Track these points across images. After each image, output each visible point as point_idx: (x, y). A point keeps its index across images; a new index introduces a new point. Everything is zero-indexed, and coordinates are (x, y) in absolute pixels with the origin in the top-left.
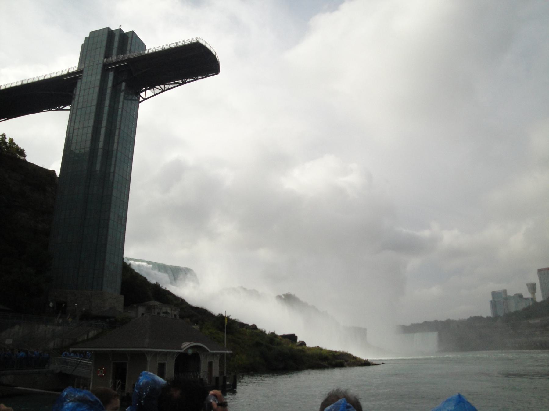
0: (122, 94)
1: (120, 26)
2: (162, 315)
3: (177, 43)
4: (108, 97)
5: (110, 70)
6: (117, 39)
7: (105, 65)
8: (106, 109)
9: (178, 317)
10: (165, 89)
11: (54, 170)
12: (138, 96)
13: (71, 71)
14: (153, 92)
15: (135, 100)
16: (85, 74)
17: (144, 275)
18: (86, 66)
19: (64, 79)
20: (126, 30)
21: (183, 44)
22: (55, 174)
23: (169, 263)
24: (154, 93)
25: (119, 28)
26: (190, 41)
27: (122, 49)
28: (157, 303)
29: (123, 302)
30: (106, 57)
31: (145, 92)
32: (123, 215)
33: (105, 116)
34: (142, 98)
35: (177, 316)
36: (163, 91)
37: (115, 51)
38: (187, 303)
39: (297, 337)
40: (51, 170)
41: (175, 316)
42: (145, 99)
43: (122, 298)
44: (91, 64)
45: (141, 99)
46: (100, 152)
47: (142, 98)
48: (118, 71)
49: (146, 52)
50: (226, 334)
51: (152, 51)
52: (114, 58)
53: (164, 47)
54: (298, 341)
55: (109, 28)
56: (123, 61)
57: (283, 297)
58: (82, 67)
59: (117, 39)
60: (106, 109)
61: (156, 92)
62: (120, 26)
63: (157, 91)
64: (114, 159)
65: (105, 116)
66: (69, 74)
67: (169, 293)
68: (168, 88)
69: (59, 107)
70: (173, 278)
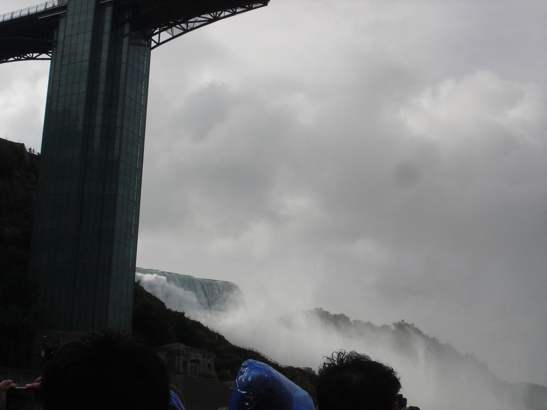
0: (126, 40)
2: (189, 364)
4: (105, 47)
5: (107, 4)
9: (214, 367)
10: (189, 28)
11: (22, 143)
12: (149, 41)
15: (144, 45)
16: (70, 11)
17: (160, 296)
22: (25, 148)
23: (199, 274)
28: (182, 347)
31: (158, 34)
32: (132, 222)
35: (212, 365)
36: (186, 31)
38: (227, 342)
39: (405, 400)
40: (19, 144)
41: (209, 365)
42: (158, 44)
45: (153, 44)
46: (98, 131)
54: (408, 405)
60: (104, 66)
61: (175, 34)
63: (176, 31)
64: (117, 141)
66: (46, 11)
67: (198, 325)
68: (192, 27)
69: (31, 54)
70: (204, 300)
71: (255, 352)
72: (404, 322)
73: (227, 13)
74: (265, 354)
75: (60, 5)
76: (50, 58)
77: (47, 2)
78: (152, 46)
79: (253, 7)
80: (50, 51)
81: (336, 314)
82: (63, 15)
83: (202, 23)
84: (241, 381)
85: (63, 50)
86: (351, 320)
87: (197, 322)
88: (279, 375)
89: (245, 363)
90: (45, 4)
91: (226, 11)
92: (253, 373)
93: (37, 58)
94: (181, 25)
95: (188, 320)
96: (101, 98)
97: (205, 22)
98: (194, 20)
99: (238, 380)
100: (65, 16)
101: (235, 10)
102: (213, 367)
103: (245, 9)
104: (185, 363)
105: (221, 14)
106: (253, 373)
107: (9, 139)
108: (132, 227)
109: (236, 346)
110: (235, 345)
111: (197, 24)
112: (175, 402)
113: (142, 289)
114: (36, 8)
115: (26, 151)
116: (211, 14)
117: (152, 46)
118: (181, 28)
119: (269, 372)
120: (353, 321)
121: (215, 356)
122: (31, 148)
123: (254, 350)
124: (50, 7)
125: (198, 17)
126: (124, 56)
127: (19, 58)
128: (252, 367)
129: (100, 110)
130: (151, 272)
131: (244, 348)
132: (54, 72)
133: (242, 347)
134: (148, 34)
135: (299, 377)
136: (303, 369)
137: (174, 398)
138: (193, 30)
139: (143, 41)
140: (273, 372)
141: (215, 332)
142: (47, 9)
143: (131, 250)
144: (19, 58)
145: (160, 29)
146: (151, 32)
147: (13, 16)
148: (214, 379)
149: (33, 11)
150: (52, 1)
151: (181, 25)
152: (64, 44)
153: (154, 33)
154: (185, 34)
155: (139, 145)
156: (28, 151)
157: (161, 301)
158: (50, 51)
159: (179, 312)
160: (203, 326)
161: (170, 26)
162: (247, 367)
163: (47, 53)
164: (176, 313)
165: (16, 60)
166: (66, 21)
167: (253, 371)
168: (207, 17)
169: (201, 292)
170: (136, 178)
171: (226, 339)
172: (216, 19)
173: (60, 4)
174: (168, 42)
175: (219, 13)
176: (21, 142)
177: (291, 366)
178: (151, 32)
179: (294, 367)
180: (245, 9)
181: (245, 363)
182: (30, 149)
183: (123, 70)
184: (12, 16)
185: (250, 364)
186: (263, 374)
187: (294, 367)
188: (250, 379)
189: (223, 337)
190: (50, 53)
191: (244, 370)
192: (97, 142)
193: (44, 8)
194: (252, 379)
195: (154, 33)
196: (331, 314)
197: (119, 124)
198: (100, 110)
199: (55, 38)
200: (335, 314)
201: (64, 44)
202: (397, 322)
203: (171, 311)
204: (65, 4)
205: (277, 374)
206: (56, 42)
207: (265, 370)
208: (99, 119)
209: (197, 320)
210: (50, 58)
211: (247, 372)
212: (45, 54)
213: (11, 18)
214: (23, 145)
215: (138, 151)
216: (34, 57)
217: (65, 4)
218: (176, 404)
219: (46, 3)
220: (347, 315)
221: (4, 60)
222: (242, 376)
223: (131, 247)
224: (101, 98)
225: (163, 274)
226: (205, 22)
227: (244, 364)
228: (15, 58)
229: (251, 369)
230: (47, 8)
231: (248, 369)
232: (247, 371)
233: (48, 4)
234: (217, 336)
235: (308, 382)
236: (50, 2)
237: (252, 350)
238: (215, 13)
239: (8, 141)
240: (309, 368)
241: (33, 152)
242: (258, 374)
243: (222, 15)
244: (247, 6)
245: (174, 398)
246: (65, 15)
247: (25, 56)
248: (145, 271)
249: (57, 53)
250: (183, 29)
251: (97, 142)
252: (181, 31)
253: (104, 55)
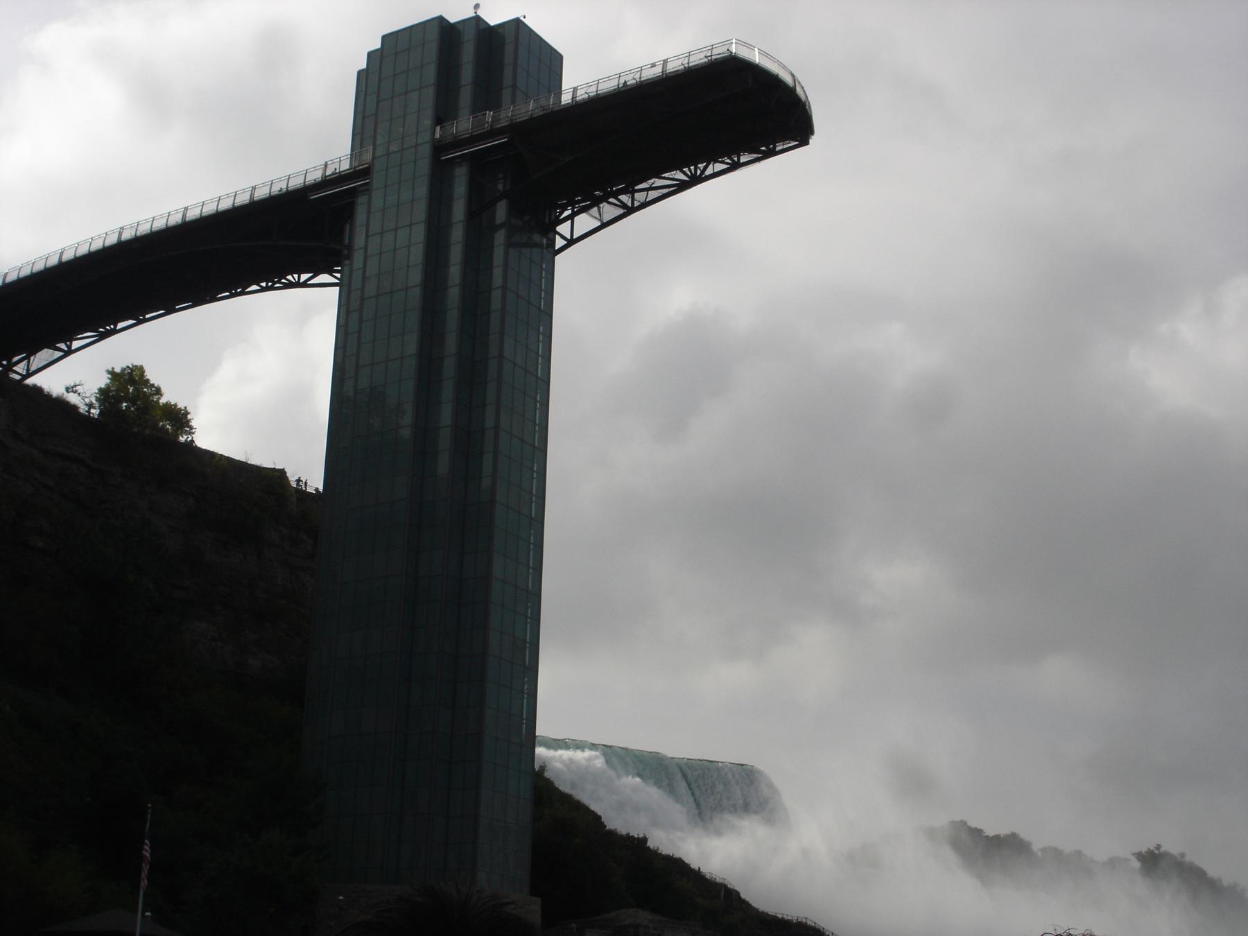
0: (500, 237)
1: (477, 6)
3: (665, 62)
6: (468, 54)
7: (439, 148)
8: (454, 293)
10: (636, 204)
11: (281, 468)
12: (551, 235)
15: (540, 246)
16: (377, 180)
18: (378, 153)
20: (494, 17)
21: (686, 66)
22: (287, 478)
25: (472, 14)
26: (706, 57)
27: (488, 94)
30: (439, 121)
34: (563, 237)
36: (629, 210)
37: (465, 96)
42: (571, 242)
44: (394, 147)
45: (560, 243)
46: (445, 438)
47: (563, 237)
48: (481, 165)
49: (566, 98)
51: (586, 96)
52: (464, 125)
53: (622, 81)
55: (441, 20)
56: (493, 133)
58: (367, 157)
59: (468, 54)
60: (454, 293)
61: (606, 218)
62: (477, 6)
66: (326, 183)
68: (642, 200)
69: (296, 276)
216: (301, 281)
246: (366, 189)
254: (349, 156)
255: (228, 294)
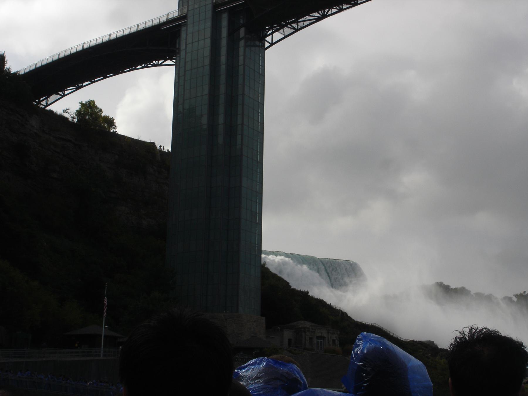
0: (242, 43)
2: (315, 341)
4: (224, 51)
5: (224, 11)
9: (338, 342)
10: (299, 27)
11: (153, 142)
12: (263, 42)
13: (171, 16)
14: (283, 33)
15: (259, 46)
16: (190, 20)
19: (163, 29)
24: (284, 35)
28: (308, 324)
29: (264, 325)
31: (271, 35)
33: (223, 78)
34: (268, 42)
35: (336, 341)
36: (296, 30)
40: (150, 142)
41: (334, 341)
42: (272, 44)
43: (263, 320)
45: (267, 45)
46: (221, 129)
47: (268, 42)
48: (232, 12)
50: (102, 335)
57: (515, 299)
58: (185, 10)
61: (287, 34)
63: (288, 31)
64: (239, 137)
65: (223, 78)
66: (169, 22)
67: (321, 303)
68: (302, 25)
69: (157, 62)
71: (377, 327)
72: (526, 293)
73: (334, 11)
74: (387, 329)
75: (180, 15)
76: (174, 63)
77: (168, 13)
78: (266, 46)
79: (359, 3)
80: (173, 58)
81: (457, 288)
82: (183, 24)
83: (311, 21)
84: (357, 353)
85: (186, 56)
86: (472, 293)
87: (321, 300)
88: (393, 346)
89: (360, 336)
90: (166, 15)
91: (333, 8)
92: (368, 345)
93: (163, 64)
94: (292, 25)
95: (312, 298)
96: (222, 99)
97: (314, 21)
98: (304, 20)
99: (354, 353)
100: (186, 24)
101: (341, 7)
102: (337, 342)
103: (351, 5)
104: (311, 339)
105: (328, 11)
106: (368, 345)
107: (142, 139)
108: (256, 215)
109: (359, 322)
110: (358, 321)
111: (306, 23)
112: (298, 376)
113: (267, 270)
114: (159, 19)
115: (157, 149)
116: (319, 12)
117: (266, 46)
118: (292, 27)
119: (384, 344)
120: (475, 294)
121: (339, 332)
122: (161, 146)
123: (376, 326)
124: (171, 17)
125: (307, 16)
126: (241, 58)
127: (146, 65)
128: (367, 340)
129: (222, 109)
130: (276, 254)
131: (367, 323)
132: (179, 77)
133: (364, 323)
134: (261, 36)
135: (421, 350)
136: (426, 343)
137: (297, 372)
138: (303, 29)
139: (257, 43)
140: (387, 343)
141: (338, 308)
142: (169, 20)
143: (257, 237)
144: (146, 65)
145: (272, 31)
146: (264, 34)
147: (139, 28)
148: (339, 355)
149: (156, 22)
150: (173, 12)
151: (292, 25)
152: (186, 51)
153: (268, 34)
154: (296, 33)
155: (259, 140)
156: (159, 148)
157: (286, 281)
158: (173, 58)
159: (304, 291)
160: (327, 303)
161: (282, 27)
162: (362, 340)
163: (171, 59)
164: (301, 292)
165: (143, 68)
166: (187, 29)
167: (368, 343)
168: (316, 15)
169: (325, 275)
170: (258, 170)
171: (349, 315)
172: (324, 17)
173: (181, 14)
174: (278, 39)
175: (326, 10)
176: (152, 141)
177: (413, 340)
178: (264, 34)
179: (416, 341)
180: (351, 5)
181: (360, 336)
182: (160, 147)
183: (241, 72)
184: (137, 28)
185: (365, 337)
186: (378, 346)
187: (416, 341)
188: (365, 351)
189: (346, 314)
190: (174, 59)
191: (359, 343)
192: (221, 140)
193: (166, 19)
194: (367, 352)
195: (268, 34)
196: (452, 288)
197: (239, 122)
198: (222, 109)
199: (178, 46)
200: (456, 288)
201: (186, 51)
202: (518, 293)
203: (296, 290)
204: (185, 13)
205: (392, 346)
206: (179, 49)
207: (380, 342)
208: (221, 119)
209: (321, 298)
210: (174, 63)
211: (363, 345)
212: (170, 61)
213: (137, 30)
214: (153, 144)
215: (258, 145)
216: (159, 63)
217: (185, 13)
218: (299, 377)
219: (168, 14)
220: (467, 288)
221: (133, 68)
222: (358, 348)
223: (256, 234)
224: (222, 99)
225: (287, 255)
226: (314, 21)
227: (359, 337)
228: (142, 65)
229: (366, 342)
230: (169, 18)
231: (363, 342)
232: (362, 344)
233: (169, 15)
234: (340, 313)
235: (430, 355)
236: (172, 12)
237: (374, 325)
238: (323, 11)
239: (140, 141)
240: (431, 341)
241: (163, 149)
242: (374, 346)
243: (330, 13)
244: (353, 2)
245: (297, 372)
246: (185, 24)
247: (152, 64)
248: (268, 253)
249: (180, 59)
250: (294, 28)
251: (221, 140)
252: (292, 31)
253: (223, 58)
254: (178, 10)
255: (128, 70)
